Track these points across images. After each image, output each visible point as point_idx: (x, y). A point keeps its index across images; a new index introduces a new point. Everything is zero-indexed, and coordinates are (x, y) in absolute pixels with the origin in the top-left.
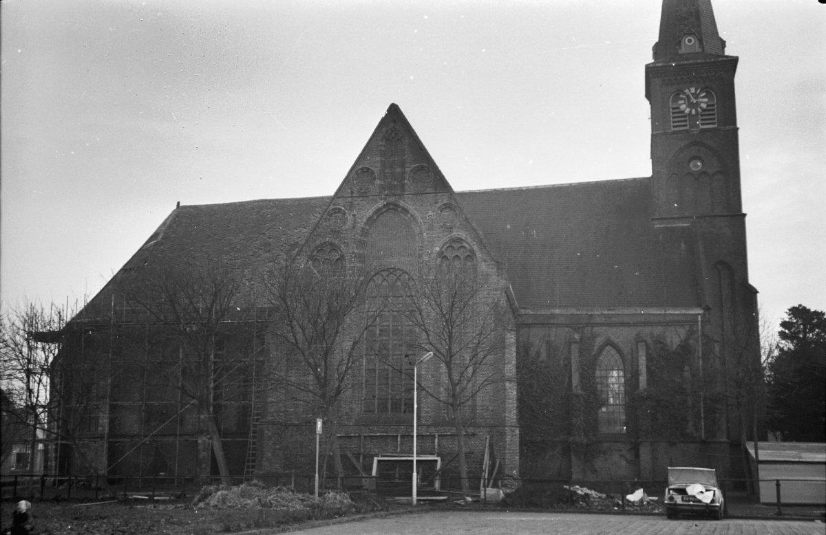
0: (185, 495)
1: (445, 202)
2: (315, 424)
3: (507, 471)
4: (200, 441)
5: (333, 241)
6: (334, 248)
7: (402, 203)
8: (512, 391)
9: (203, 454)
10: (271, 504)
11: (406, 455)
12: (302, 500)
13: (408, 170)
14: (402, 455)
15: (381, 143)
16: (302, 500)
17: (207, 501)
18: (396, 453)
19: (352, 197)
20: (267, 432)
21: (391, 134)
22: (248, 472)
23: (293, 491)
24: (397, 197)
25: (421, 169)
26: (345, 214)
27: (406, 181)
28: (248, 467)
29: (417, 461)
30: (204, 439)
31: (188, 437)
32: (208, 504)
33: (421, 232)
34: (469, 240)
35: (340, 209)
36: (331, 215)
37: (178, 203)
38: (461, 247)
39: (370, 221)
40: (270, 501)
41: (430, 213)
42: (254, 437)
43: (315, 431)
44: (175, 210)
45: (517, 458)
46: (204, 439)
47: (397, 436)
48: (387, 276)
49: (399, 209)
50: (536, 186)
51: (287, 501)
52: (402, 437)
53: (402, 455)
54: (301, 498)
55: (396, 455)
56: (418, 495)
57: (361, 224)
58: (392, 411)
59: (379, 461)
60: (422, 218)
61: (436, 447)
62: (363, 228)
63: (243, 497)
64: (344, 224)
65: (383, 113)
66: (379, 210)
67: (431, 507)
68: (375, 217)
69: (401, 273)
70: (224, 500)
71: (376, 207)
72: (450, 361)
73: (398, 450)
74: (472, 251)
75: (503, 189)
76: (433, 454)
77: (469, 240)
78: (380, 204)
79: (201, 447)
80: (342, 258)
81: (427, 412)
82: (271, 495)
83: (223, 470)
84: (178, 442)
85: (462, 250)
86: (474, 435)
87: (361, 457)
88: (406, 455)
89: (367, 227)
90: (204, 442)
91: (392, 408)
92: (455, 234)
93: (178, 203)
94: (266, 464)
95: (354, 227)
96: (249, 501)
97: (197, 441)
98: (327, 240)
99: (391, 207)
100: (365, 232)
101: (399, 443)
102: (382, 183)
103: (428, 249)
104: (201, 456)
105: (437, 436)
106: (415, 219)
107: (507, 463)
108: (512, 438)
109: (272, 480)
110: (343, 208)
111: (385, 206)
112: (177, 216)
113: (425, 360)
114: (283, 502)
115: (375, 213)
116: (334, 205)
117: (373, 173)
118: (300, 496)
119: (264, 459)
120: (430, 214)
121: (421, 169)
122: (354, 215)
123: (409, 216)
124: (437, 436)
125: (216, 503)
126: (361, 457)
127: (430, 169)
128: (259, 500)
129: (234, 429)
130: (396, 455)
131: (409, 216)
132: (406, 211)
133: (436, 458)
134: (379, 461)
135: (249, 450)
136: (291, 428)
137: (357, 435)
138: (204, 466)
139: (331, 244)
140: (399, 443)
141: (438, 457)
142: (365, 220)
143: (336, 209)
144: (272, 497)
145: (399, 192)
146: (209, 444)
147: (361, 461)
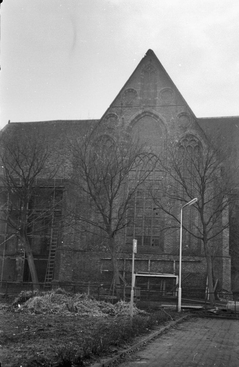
0: (7, 296)
1: (182, 112)
2: (132, 244)
3: (223, 287)
4: (17, 260)
5: (109, 134)
6: (109, 138)
7: (154, 112)
8: (226, 234)
9: (19, 268)
10: (76, 309)
11: (154, 273)
12: (100, 306)
13: (159, 91)
14: (151, 273)
15: (141, 74)
16: (100, 306)
17: (26, 304)
18: (148, 272)
19: (122, 107)
20: (62, 254)
21: (148, 68)
22: (47, 280)
23: (92, 299)
24: (151, 108)
25: (166, 91)
26: (117, 117)
27: (157, 98)
28: (47, 277)
29: (50, 268)
30: (20, 258)
31: (10, 257)
32: (26, 307)
33: (166, 130)
34: (198, 136)
35: (114, 115)
36: (108, 119)
37: (9, 121)
38: (192, 140)
39: (133, 122)
40: (76, 307)
41: (173, 118)
42: (51, 258)
43: (132, 251)
44: (7, 125)
45: (230, 278)
46: (20, 258)
47: (148, 260)
48: (143, 158)
49: (152, 116)
50: (222, 117)
51: (89, 307)
52: (151, 261)
53: (151, 273)
54: (99, 304)
55: (148, 273)
56: (182, 305)
57: (127, 124)
58: (144, 245)
59: (136, 277)
60: (167, 122)
61: (174, 269)
62: (128, 127)
63: (53, 302)
64: (116, 124)
65: (143, 54)
66: (139, 115)
67: (192, 314)
68: (136, 120)
69: (152, 155)
70: (39, 304)
71: (137, 114)
72: (202, 208)
73: (149, 270)
74: (200, 143)
75: (202, 118)
76: (172, 273)
77: (198, 136)
78: (140, 112)
79: (17, 263)
80: (114, 145)
81: (168, 246)
82: (75, 302)
83: (35, 280)
84: (3, 260)
85: (193, 142)
86: (199, 262)
87: (124, 273)
88: (154, 273)
89: (131, 127)
90: (20, 260)
91: (144, 243)
92: (188, 131)
93: (9, 121)
94: (61, 276)
95: (122, 126)
96: (58, 306)
97: (15, 259)
98: (105, 134)
99: (147, 114)
100: (129, 130)
101: (149, 265)
102: (141, 98)
103: (170, 141)
104: (17, 269)
105: (174, 261)
106: (162, 122)
107: (223, 281)
108: (227, 265)
109: (73, 288)
110: (116, 114)
111: (143, 113)
112: (9, 128)
113: (190, 205)
114: (86, 308)
115: (136, 118)
116: (110, 112)
117: (136, 92)
118: (98, 303)
119: (60, 272)
120: (173, 119)
121: (166, 91)
122: (123, 118)
123: (158, 120)
124: (174, 261)
125: (33, 306)
126: (124, 273)
127: (173, 90)
128: (67, 305)
129: (39, 253)
130: (148, 273)
131: (158, 120)
132: (156, 117)
133: (176, 276)
134: (136, 277)
135: (48, 266)
136: (78, 253)
137: (121, 259)
138: (19, 275)
139: (107, 136)
140: (149, 265)
141: (176, 275)
142: (130, 122)
143: (111, 114)
144: (77, 303)
145: (153, 105)
146: (23, 262)
147: (124, 276)
